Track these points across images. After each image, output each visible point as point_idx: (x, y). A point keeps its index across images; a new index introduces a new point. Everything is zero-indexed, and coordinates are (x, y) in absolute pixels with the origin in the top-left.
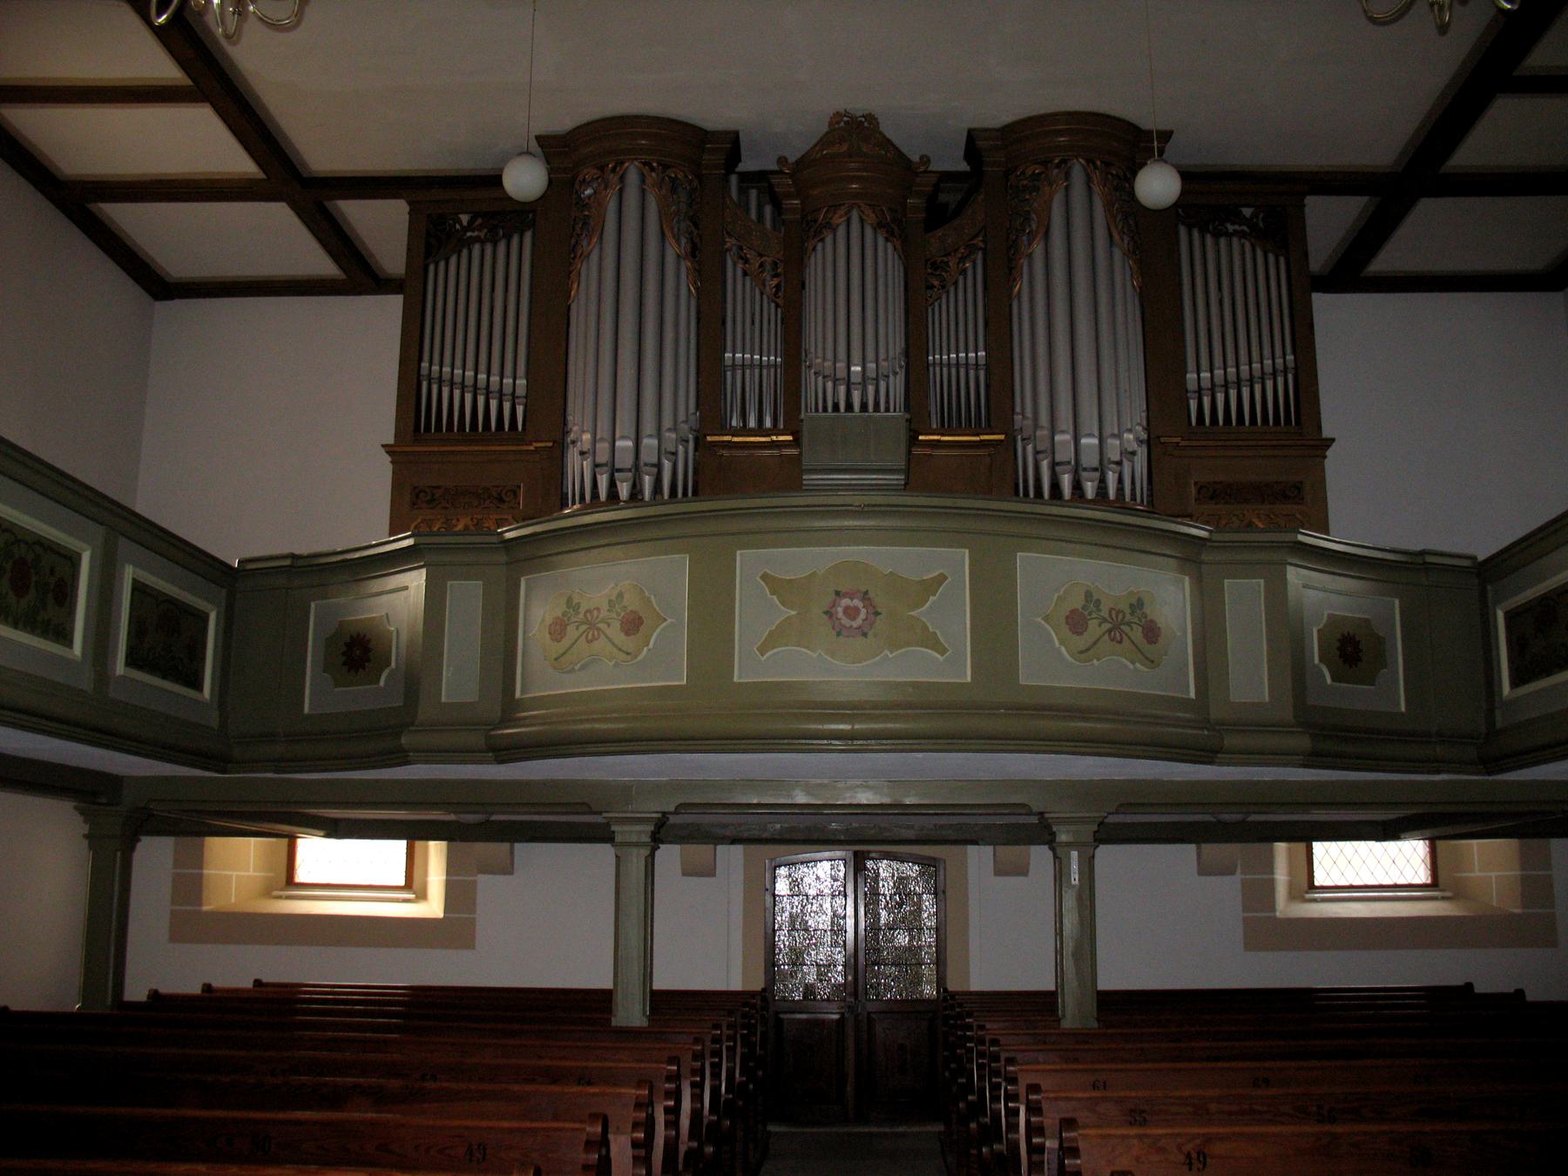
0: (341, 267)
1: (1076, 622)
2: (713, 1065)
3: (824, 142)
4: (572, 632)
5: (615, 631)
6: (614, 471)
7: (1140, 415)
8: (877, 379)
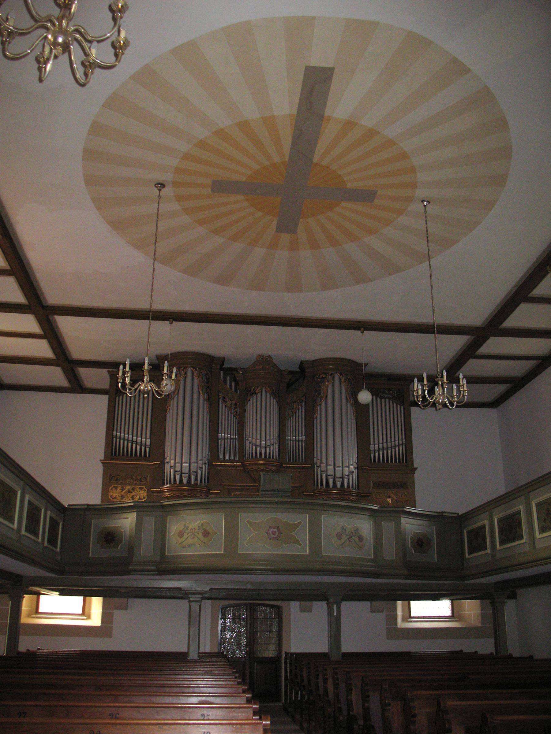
0: (28, 301)
1: (339, 536)
3: (254, 364)
4: (186, 536)
5: (200, 536)
7: (355, 455)
8: (270, 446)
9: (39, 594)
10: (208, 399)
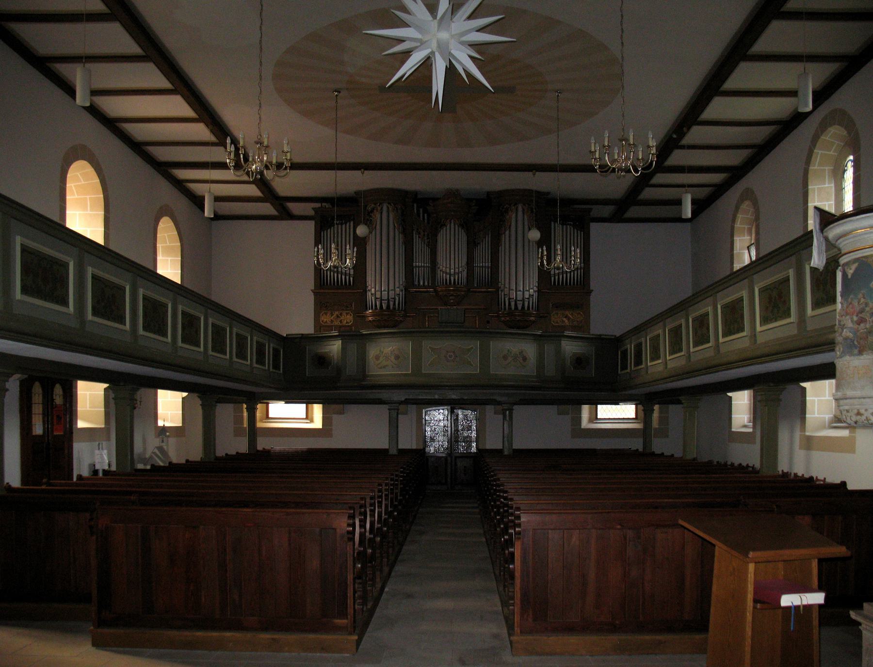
2: (371, 510)
4: (381, 359)
5: (393, 358)
6: (381, 300)
7: (536, 279)
9: (268, 404)
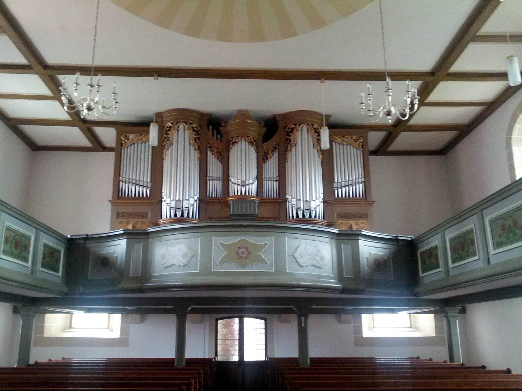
0: (28, 61)
7: (321, 191)
10: (198, 149)
